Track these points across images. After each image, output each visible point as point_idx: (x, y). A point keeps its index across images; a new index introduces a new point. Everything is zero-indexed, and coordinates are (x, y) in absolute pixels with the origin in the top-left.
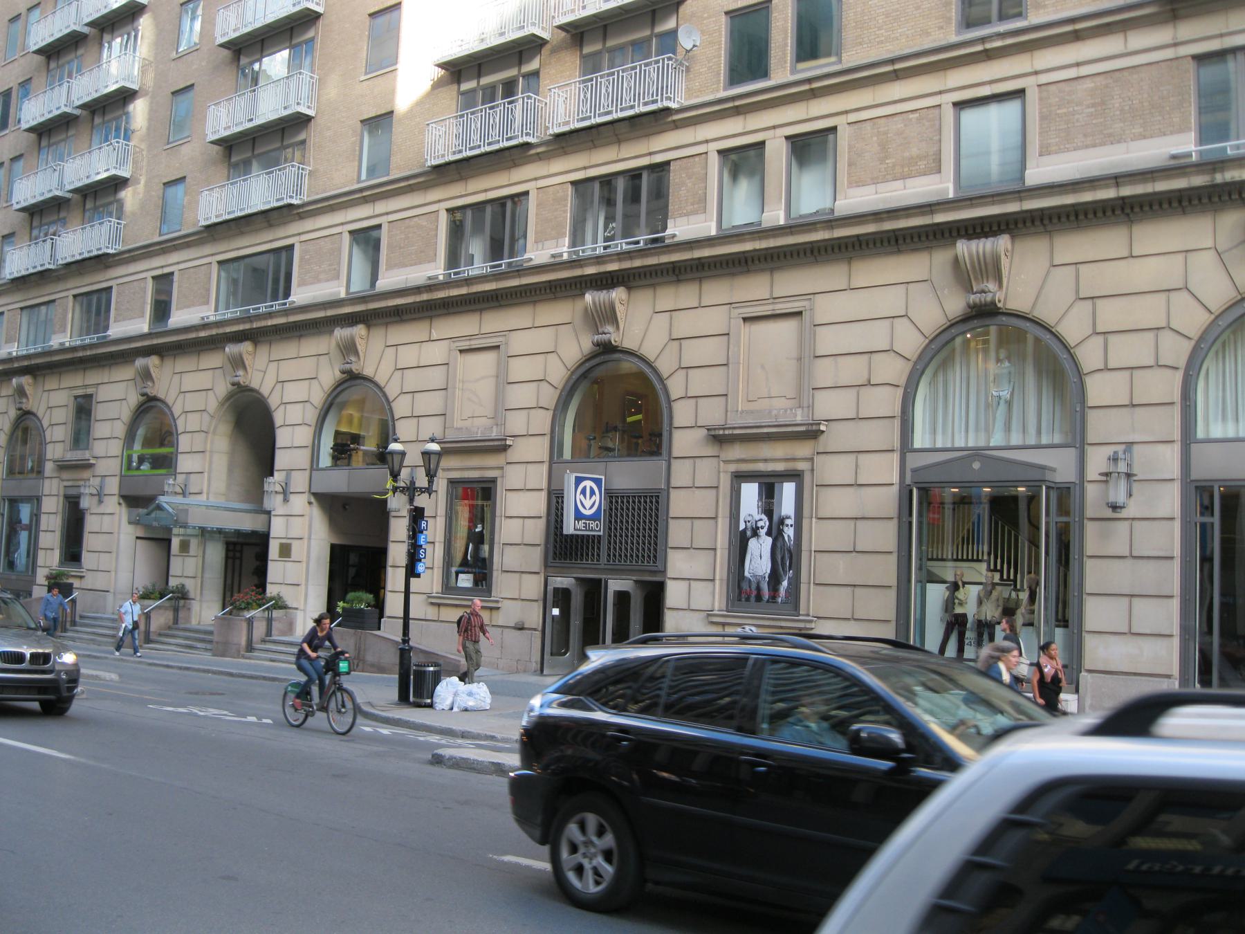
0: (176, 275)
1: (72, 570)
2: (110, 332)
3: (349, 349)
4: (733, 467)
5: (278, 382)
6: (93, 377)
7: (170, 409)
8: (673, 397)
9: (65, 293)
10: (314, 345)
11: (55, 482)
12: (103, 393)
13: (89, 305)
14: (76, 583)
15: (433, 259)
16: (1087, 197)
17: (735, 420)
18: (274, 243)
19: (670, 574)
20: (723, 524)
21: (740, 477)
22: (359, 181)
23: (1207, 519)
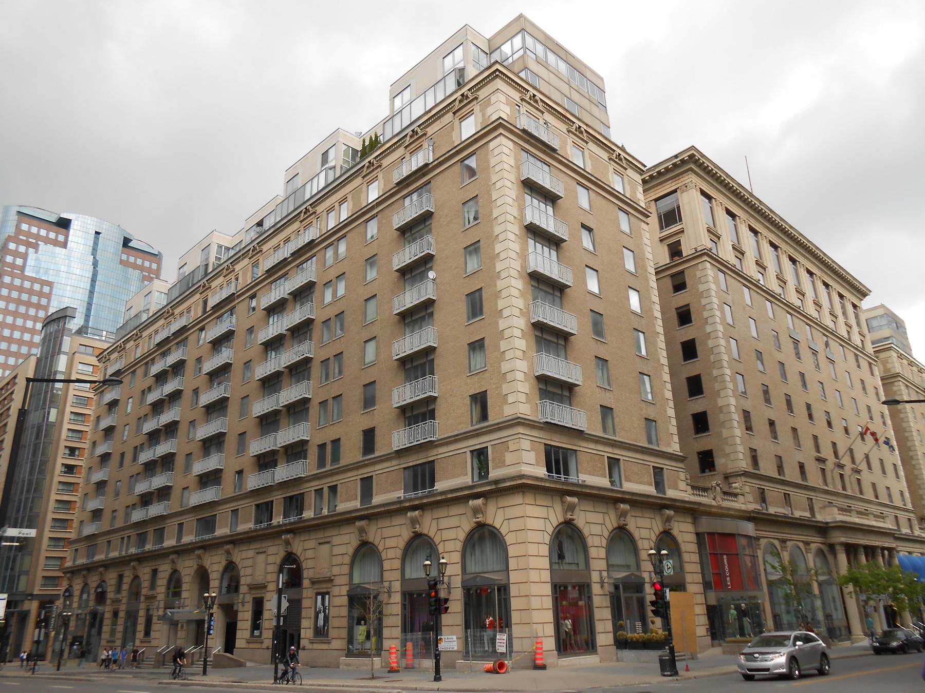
0: (374, 477)
3: (228, 552)
4: (315, 591)
10: (398, 520)
11: (310, 590)
12: (161, 568)
15: (251, 522)
20: (313, 609)
21: (317, 594)
22: (235, 492)
23: (505, 597)
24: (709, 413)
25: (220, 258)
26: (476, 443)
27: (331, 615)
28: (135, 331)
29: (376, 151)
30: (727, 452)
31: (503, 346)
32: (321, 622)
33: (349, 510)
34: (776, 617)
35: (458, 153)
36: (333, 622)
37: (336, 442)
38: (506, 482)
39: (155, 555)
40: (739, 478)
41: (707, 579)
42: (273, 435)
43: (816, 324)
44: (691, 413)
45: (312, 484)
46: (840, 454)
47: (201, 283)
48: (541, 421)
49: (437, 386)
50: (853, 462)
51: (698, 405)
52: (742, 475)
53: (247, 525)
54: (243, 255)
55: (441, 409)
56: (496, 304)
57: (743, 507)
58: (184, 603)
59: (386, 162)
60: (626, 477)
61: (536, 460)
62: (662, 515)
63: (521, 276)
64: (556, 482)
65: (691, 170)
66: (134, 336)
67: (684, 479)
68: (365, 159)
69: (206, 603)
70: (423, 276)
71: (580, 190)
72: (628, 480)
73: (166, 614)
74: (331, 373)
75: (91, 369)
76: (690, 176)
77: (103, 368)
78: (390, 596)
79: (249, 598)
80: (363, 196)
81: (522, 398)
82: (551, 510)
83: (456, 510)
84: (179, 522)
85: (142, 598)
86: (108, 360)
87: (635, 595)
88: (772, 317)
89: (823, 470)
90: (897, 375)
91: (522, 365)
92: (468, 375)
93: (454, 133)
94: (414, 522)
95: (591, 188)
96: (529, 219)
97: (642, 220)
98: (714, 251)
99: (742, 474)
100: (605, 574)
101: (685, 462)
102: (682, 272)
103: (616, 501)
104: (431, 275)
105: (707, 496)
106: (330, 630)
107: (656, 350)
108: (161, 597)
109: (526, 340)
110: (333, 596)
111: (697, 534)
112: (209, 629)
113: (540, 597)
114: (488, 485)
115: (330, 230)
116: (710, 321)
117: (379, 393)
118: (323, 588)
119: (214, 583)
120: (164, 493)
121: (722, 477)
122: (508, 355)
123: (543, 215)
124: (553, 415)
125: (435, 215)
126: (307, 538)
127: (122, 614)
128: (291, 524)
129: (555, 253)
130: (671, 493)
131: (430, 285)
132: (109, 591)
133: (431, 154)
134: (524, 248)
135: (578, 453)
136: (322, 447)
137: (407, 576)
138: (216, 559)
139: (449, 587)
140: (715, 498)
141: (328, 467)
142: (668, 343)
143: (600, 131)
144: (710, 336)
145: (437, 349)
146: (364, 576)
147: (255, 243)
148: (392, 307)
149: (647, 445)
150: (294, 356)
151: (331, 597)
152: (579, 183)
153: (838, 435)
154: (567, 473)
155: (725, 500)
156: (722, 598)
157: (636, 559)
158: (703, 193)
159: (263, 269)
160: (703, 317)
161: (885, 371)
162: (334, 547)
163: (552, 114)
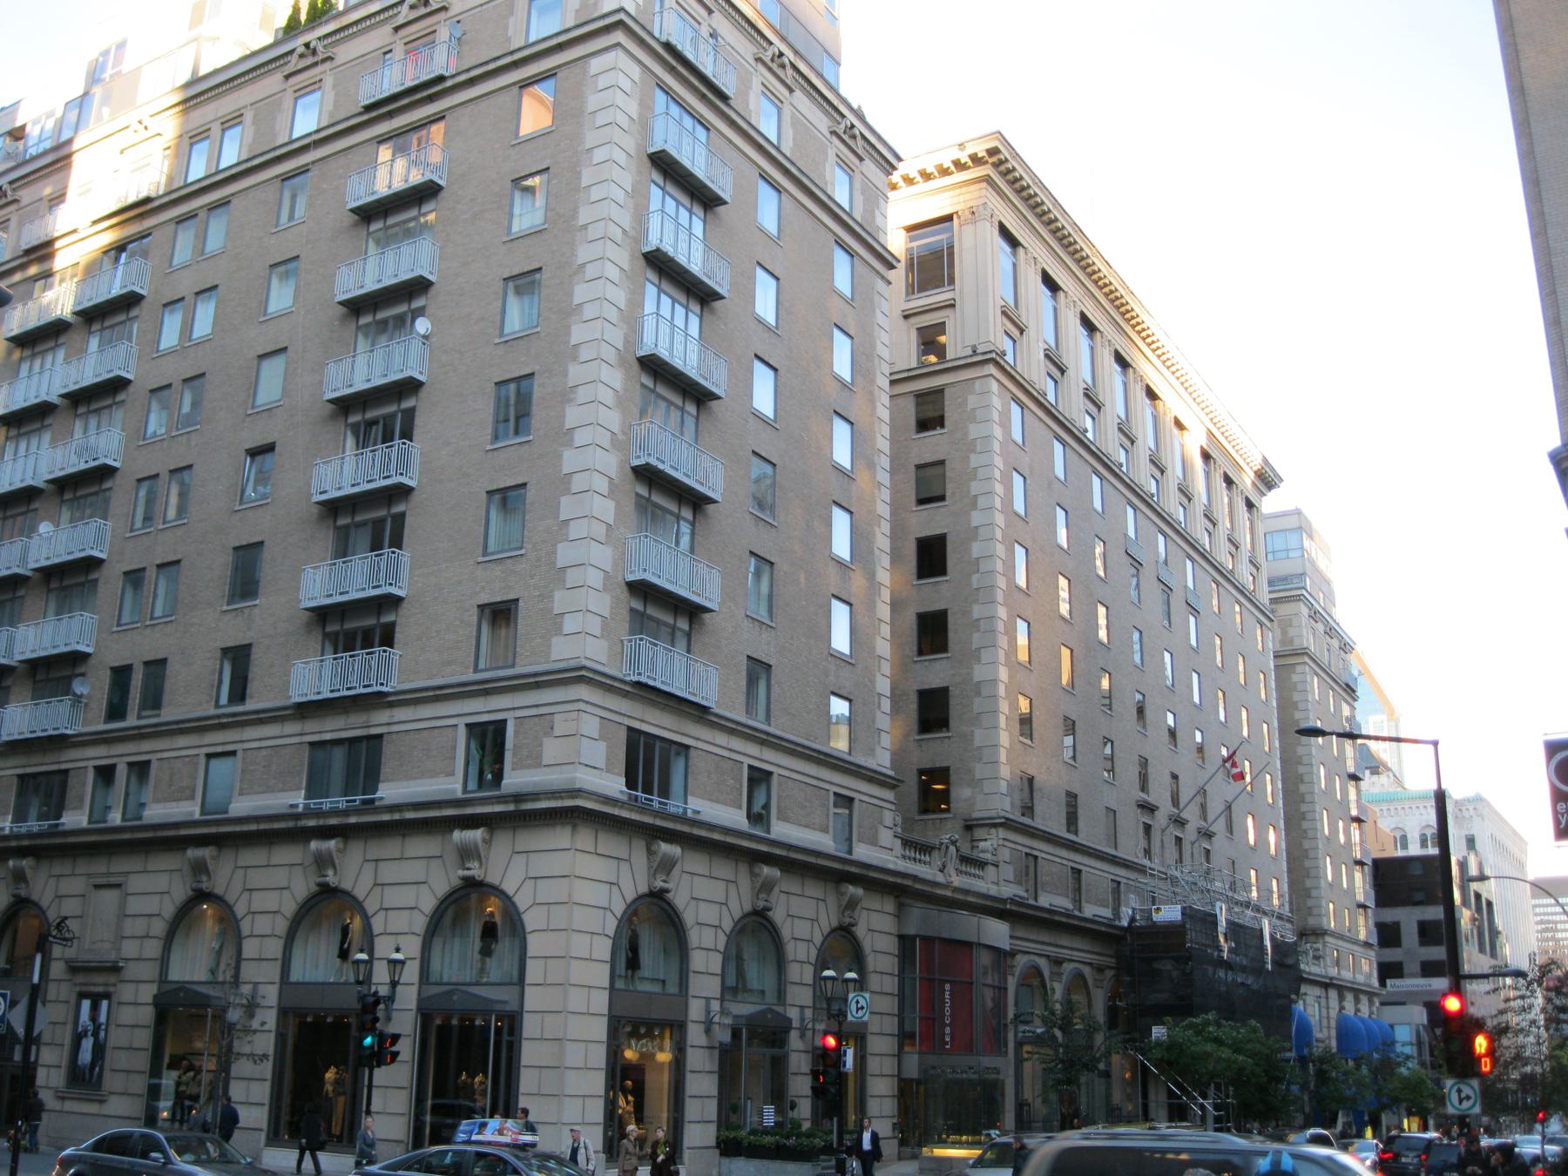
3: (200, 868)
4: (78, 989)
5: (376, 885)
10: (287, 854)
16: (277, 825)
18: (589, 706)
20: (69, 1027)
21: (82, 995)
24: (953, 691)
27: (111, 1042)
29: (327, 22)
30: (978, 776)
31: (567, 508)
32: (86, 1056)
33: (173, 820)
34: (1021, 1105)
35: (516, 65)
37: (157, 667)
40: (993, 831)
41: (907, 1028)
43: (1178, 532)
44: (916, 688)
45: (91, 752)
46: (1183, 799)
48: (628, 679)
50: (1204, 816)
51: (935, 673)
52: (1001, 825)
55: (407, 624)
56: (562, 416)
57: (993, 891)
59: (346, 52)
60: (779, 810)
61: (608, 759)
62: (841, 894)
63: (622, 362)
67: (892, 826)
70: (402, 323)
71: (764, 191)
72: (783, 817)
78: (252, 1016)
80: (282, 121)
81: (595, 626)
82: (624, 867)
83: (419, 846)
87: (769, 1052)
88: (1100, 509)
89: (1148, 828)
90: (1304, 652)
91: (602, 556)
92: (481, 559)
93: (512, 20)
95: (786, 190)
96: (653, 242)
97: (878, 272)
98: (1009, 358)
99: (1001, 825)
100: (715, 1006)
101: (897, 789)
102: (939, 392)
104: (422, 326)
106: (107, 1075)
107: (872, 552)
109: (617, 503)
110: (119, 1003)
111: (902, 938)
113: (583, 1045)
114: (499, 803)
115: (192, 184)
116: (982, 502)
117: (268, 571)
118: (98, 983)
121: (959, 824)
122: (576, 530)
125: (442, 195)
128: (31, 835)
131: (416, 344)
134: (636, 302)
135: (692, 752)
136: (121, 674)
137: (295, 976)
140: (944, 866)
141: (131, 721)
142: (895, 537)
148: (321, 382)
150: (74, 459)
151: (114, 1006)
152: (764, 177)
153: (1184, 762)
154: (665, 792)
155: (961, 872)
156: (934, 1068)
157: (779, 979)
158: (1004, 232)
160: (969, 492)
161: (1283, 642)
162: (129, 897)
163: (809, 95)
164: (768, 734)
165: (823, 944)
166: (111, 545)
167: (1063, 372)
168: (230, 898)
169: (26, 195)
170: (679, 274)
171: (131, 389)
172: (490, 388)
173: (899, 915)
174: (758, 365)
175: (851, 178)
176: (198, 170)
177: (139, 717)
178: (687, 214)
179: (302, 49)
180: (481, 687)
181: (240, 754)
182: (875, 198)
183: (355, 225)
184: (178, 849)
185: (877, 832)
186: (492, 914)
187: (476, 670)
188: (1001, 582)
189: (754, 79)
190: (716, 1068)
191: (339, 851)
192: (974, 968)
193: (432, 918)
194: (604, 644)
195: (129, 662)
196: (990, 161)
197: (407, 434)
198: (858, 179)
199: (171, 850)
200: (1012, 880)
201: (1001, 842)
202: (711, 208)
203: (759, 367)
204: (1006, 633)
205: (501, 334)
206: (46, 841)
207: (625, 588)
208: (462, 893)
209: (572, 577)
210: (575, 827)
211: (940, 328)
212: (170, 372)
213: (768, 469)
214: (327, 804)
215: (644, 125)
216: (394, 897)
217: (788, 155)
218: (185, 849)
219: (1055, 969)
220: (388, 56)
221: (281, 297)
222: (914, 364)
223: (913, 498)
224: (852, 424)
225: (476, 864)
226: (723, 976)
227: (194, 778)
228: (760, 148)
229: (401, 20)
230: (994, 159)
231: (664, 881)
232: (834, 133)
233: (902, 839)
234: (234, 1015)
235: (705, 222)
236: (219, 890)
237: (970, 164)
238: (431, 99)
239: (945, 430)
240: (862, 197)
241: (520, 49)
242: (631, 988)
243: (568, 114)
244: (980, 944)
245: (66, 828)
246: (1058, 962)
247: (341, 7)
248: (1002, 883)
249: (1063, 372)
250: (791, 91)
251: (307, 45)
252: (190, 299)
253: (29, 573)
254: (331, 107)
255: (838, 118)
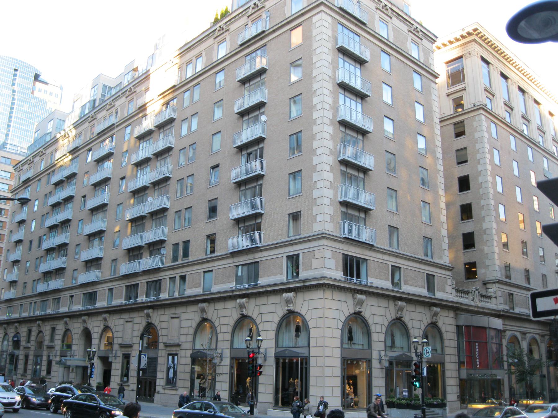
1: (48, 376)
2: (60, 310)
3: (203, 310)
4: (168, 352)
5: (259, 314)
6: (56, 323)
7: (156, 327)
8: (218, 333)
9: (51, 298)
10: (230, 304)
11: (164, 352)
13: (156, 285)
14: (47, 380)
15: (122, 298)
16: (226, 295)
17: (169, 342)
19: (157, 377)
20: (166, 365)
21: (169, 355)
22: (111, 276)
24: (476, 234)
25: (105, 96)
26: (291, 250)
27: (178, 370)
28: (41, 149)
29: (226, 18)
31: (316, 177)
32: (171, 375)
34: (511, 389)
35: (288, 23)
36: (180, 376)
37: (186, 243)
38: (311, 281)
39: (53, 318)
40: (494, 285)
41: (462, 360)
42: (140, 235)
47: (90, 114)
48: (341, 236)
49: (263, 205)
51: (468, 227)
52: (497, 282)
53: (119, 301)
54: (121, 94)
55: (265, 222)
57: (495, 307)
58: (74, 353)
59: (233, 27)
63: (332, 123)
64: (349, 283)
65: (474, 41)
66: (40, 153)
68: (216, 24)
69: (89, 356)
70: (257, 118)
71: (383, 55)
72: (406, 283)
73: (61, 360)
74: (184, 190)
75: (9, 175)
76: (473, 46)
77: (18, 176)
79: (120, 354)
81: (328, 218)
82: (344, 304)
83: (273, 299)
84: (71, 295)
85: (45, 347)
86: (22, 170)
88: (532, 160)
91: (329, 193)
92: (288, 198)
93: (286, 7)
94: (242, 306)
95: (392, 54)
97: (432, 80)
99: (497, 282)
100: (383, 353)
102: (462, 122)
103: (396, 299)
104: (263, 118)
105: (468, 298)
106: (178, 381)
108: (58, 348)
111: (458, 327)
112: (91, 374)
113: (332, 368)
116: (481, 162)
118: (174, 350)
119: (95, 341)
120: (60, 271)
121: (480, 283)
122: (319, 185)
123: (353, 76)
124: (351, 232)
126: (163, 313)
127: (31, 358)
128: (151, 302)
129: (361, 105)
130: (439, 295)
131: (262, 126)
132: (22, 340)
133: (268, 23)
135: (368, 261)
136: (176, 245)
137: (235, 346)
138: (96, 323)
139: (265, 356)
141: (180, 262)
142: (446, 178)
143: (402, 9)
144: (481, 174)
145: (265, 177)
146: (202, 343)
147: (131, 86)
149: (423, 257)
150: (157, 175)
151: (179, 357)
154: (358, 276)
155: (481, 301)
156: (471, 375)
158: (483, 59)
159: (136, 106)
160: (476, 158)
162: (182, 321)
163: (398, 19)
164: (398, 253)
165: (425, 329)
166: (171, 203)
167: (512, 109)
168: (213, 320)
169: (138, 90)
170: (352, 90)
171: (174, 150)
172: (288, 137)
173: (456, 318)
174: (385, 119)
175: (418, 47)
176: (190, 74)
177: (182, 260)
178: (354, 67)
179: (219, 28)
180: (290, 243)
181: (214, 271)
182: (428, 53)
183: (240, 86)
184: (196, 304)
185: (445, 287)
186: (298, 322)
187: (289, 237)
188: (491, 191)
189: (376, 16)
190: (384, 376)
191: (247, 302)
192: (488, 337)
193: (278, 325)
194: (332, 224)
195: (178, 242)
196: (475, 33)
197: (261, 156)
198: (421, 46)
199: (194, 304)
200: (503, 303)
201: (497, 289)
202: (363, 64)
203: (386, 120)
204: (495, 210)
205: (290, 118)
206: (155, 304)
207: (339, 204)
208: (288, 315)
209: (319, 201)
210: (324, 290)
211: (461, 98)
212: (186, 143)
213: (392, 156)
214: (242, 287)
215: (334, 38)
216: (266, 318)
217: (392, 42)
218: (198, 304)
219: (523, 336)
220: (246, 27)
221: (218, 114)
222: (452, 113)
223: (456, 162)
224: (425, 137)
225: (292, 305)
226: (385, 342)
227: (200, 280)
228: (380, 41)
229: (250, 13)
230: (476, 32)
231: (360, 308)
232: (410, 31)
233: (456, 289)
234: (216, 361)
235: (361, 70)
236: (209, 318)
237: (467, 35)
238: (261, 39)
239: (466, 136)
240: (423, 54)
241: (289, 17)
242: (350, 347)
243: (307, 37)
244: (489, 328)
245: (162, 299)
246: (524, 334)
247: (231, 12)
248: (499, 304)
249: (512, 109)
250: (391, 18)
251: (220, 27)
252: (190, 118)
253: (146, 215)
254: (230, 47)
255: (411, 25)
